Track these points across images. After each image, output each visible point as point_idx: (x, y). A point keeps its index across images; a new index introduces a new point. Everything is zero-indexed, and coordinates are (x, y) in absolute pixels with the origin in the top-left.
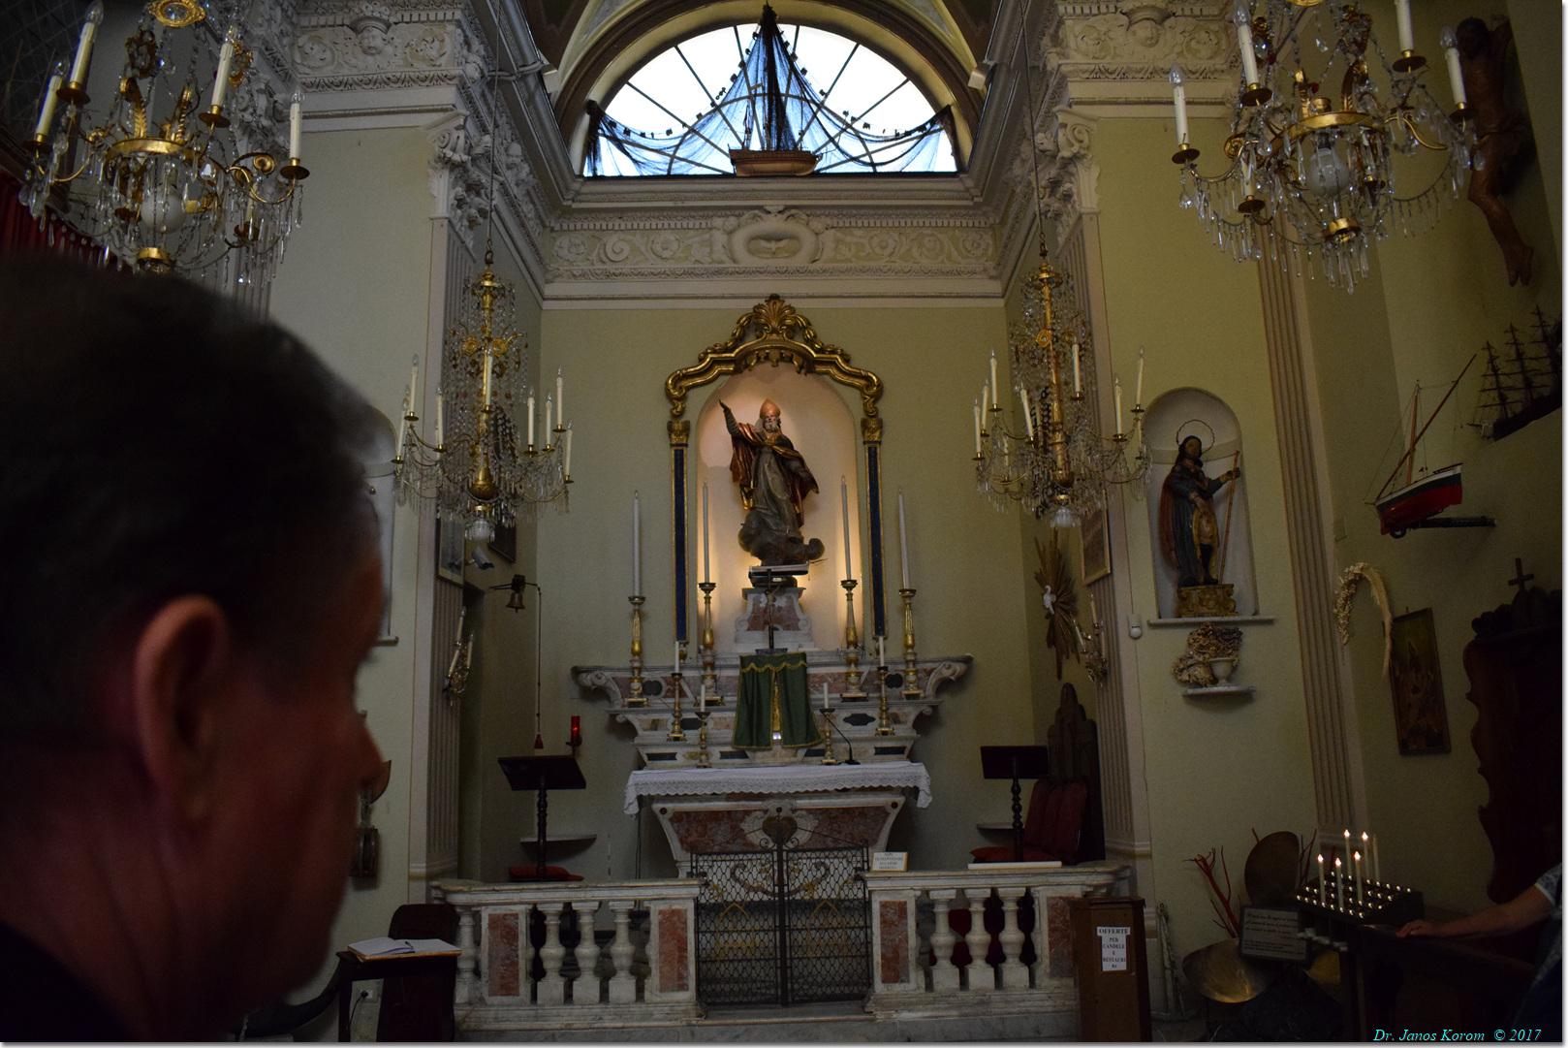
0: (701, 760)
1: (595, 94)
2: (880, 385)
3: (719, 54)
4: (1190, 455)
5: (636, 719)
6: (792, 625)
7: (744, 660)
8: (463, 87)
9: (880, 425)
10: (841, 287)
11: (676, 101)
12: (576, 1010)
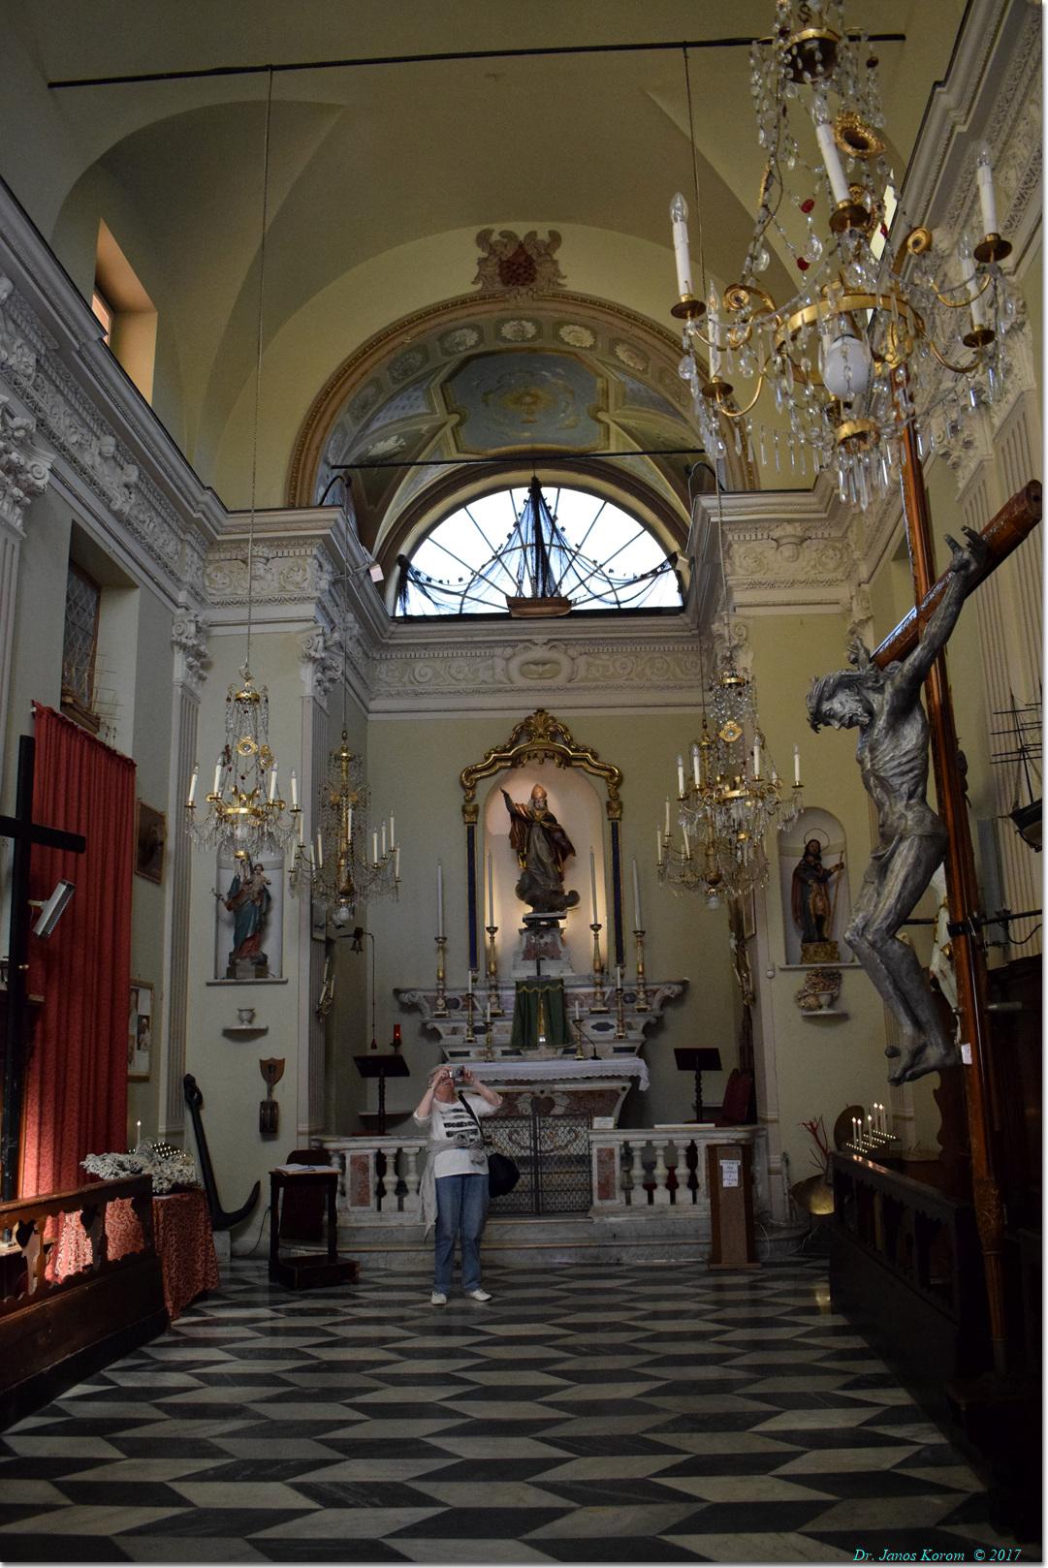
0: (487, 1056)
1: (404, 551)
2: (621, 777)
3: (497, 513)
4: (813, 852)
5: (440, 1027)
6: (555, 956)
7: (519, 985)
8: (320, 604)
9: (621, 806)
10: (591, 699)
11: (467, 554)
12: (405, 1215)
